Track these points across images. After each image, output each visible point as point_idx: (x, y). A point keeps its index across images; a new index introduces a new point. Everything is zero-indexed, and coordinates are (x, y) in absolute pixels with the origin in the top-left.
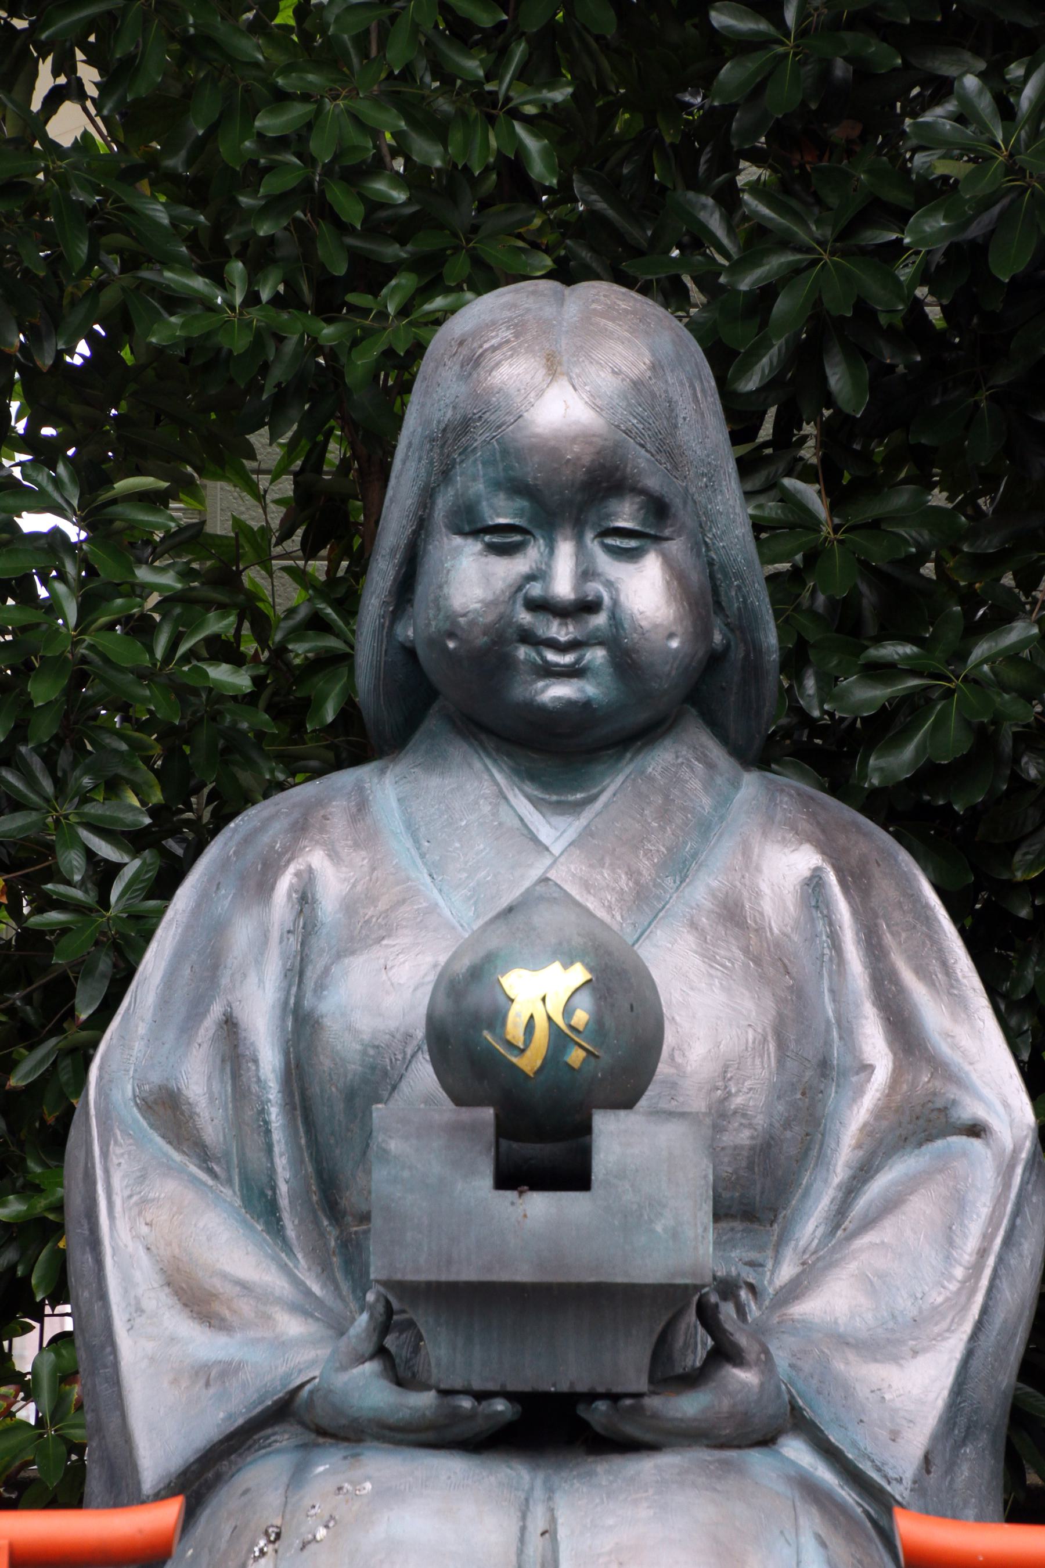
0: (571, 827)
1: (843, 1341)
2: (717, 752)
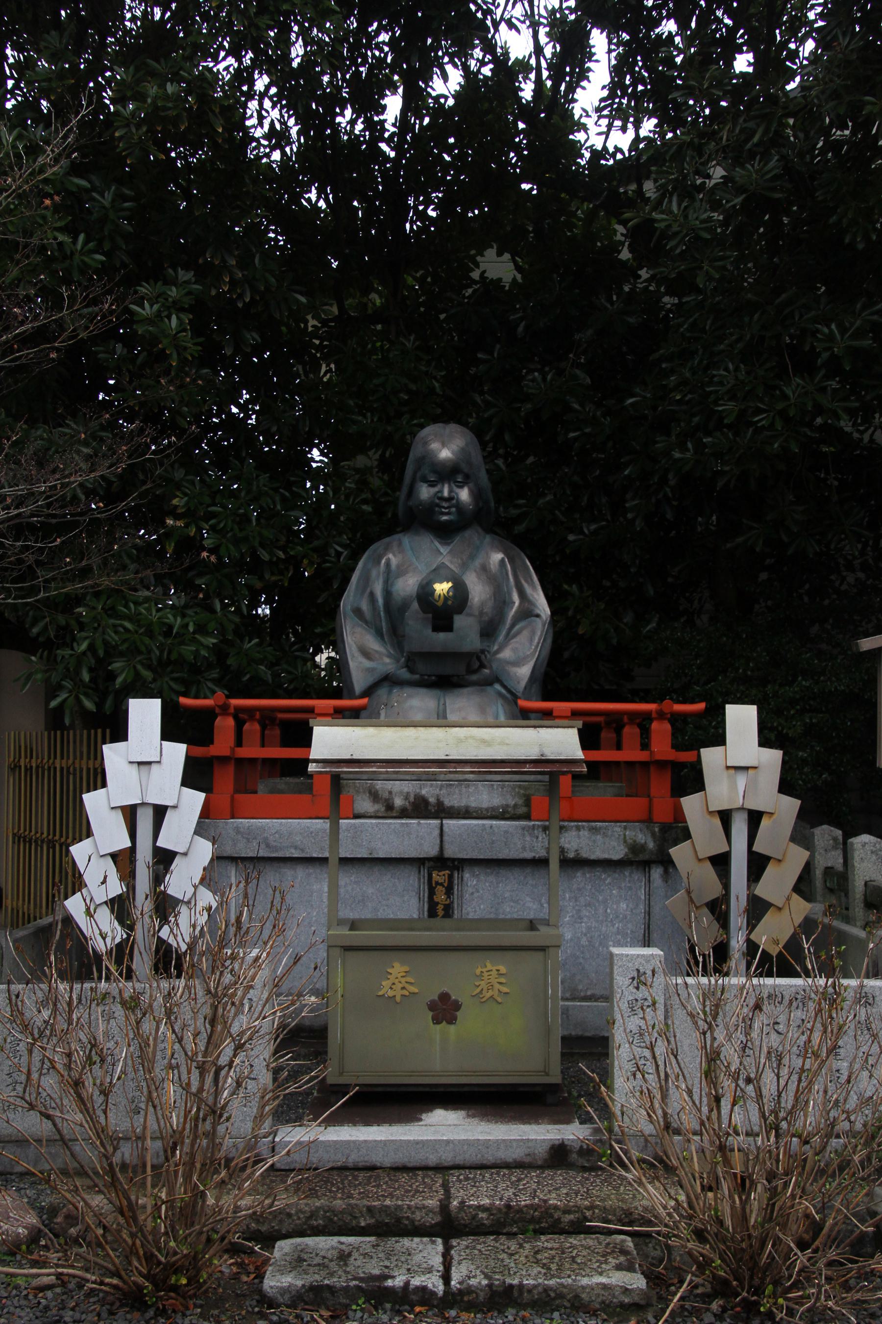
0: (448, 548)
1: (509, 663)
2: (480, 530)
